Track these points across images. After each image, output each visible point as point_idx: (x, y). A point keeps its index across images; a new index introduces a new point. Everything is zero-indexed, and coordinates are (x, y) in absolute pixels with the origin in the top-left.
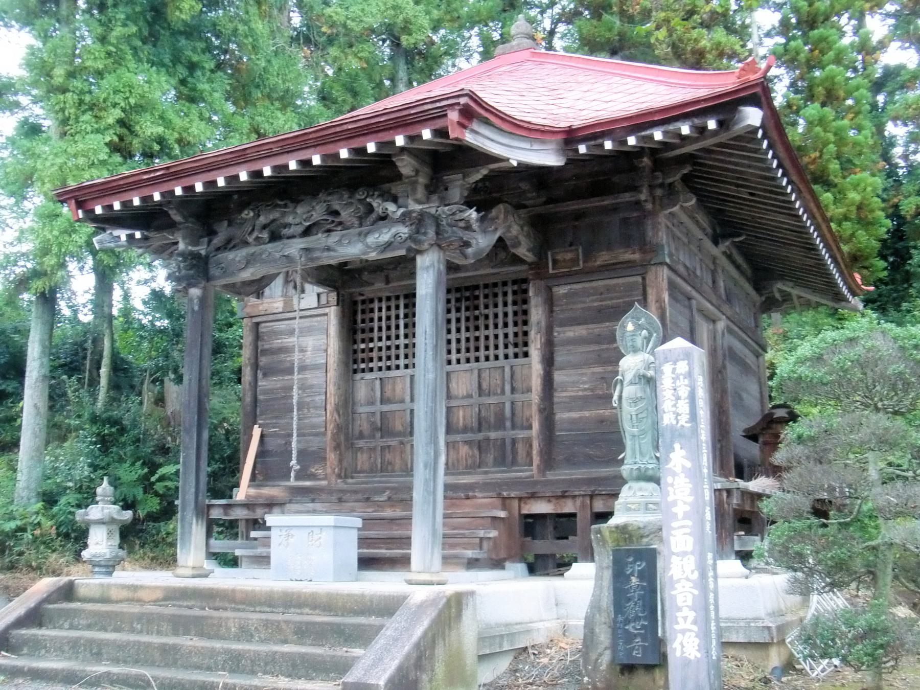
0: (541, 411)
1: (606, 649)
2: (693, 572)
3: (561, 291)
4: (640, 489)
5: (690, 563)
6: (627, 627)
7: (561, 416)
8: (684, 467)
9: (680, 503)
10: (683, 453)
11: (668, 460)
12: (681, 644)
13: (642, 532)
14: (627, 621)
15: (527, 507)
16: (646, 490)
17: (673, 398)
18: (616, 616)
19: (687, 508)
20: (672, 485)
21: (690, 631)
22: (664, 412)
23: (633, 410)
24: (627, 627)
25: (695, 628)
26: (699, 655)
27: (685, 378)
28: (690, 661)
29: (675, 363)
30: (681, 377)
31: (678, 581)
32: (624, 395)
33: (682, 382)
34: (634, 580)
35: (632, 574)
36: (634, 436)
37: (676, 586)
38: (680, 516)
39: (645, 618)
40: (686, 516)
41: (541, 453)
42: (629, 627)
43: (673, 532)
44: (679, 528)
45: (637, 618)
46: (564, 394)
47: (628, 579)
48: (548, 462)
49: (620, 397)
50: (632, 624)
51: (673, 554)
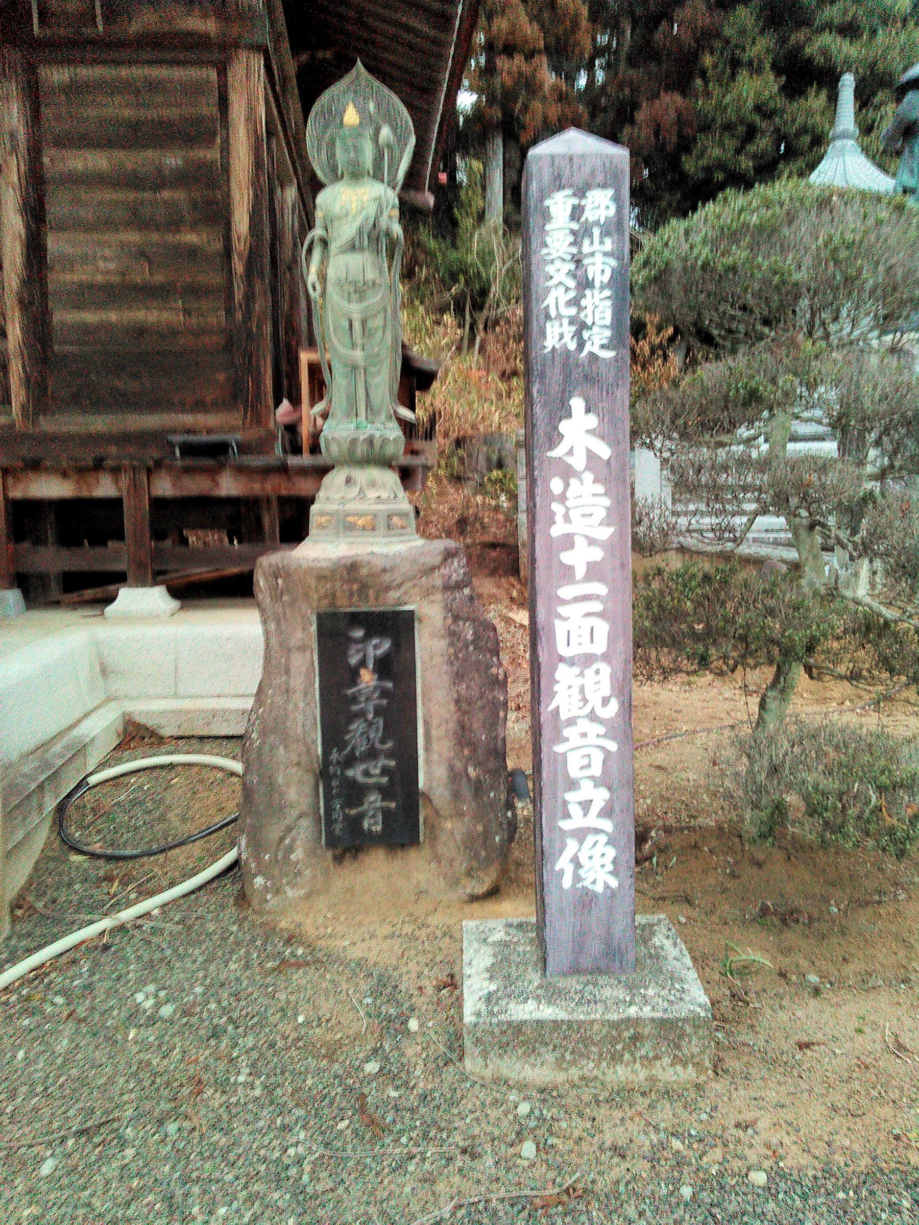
0: (24, 305)
1: (300, 816)
2: (605, 702)
3: (56, 76)
4: (373, 484)
5: (600, 682)
6: (350, 773)
7: (63, 317)
8: (591, 456)
9: (580, 542)
10: (592, 421)
11: (555, 438)
12: (576, 862)
13: (387, 578)
14: (350, 761)
15: (21, 486)
16: (384, 486)
17: (572, 283)
18: (326, 752)
19: (597, 554)
20: (563, 498)
21: (597, 831)
22: (548, 317)
23: (355, 310)
24: (350, 773)
25: (607, 825)
26: (614, 883)
27: (605, 233)
28: (596, 895)
29: (581, 193)
30: (596, 232)
31: (572, 722)
32: (331, 273)
33: (596, 246)
34: (367, 678)
35: (363, 663)
36: (354, 368)
37: (566, 732)
38: (580, 572)
39: (390, 755)
40: (594, 572)
41: (27, 381)
42: (355, 773)
43: (561, 610)
44: (577, 599)
45: (372, 754)
46: (68, 277)
47: (354, 675)
48: (41, 400)
49: (323, 277)
50: (363, 767)
51: (561, 659)
